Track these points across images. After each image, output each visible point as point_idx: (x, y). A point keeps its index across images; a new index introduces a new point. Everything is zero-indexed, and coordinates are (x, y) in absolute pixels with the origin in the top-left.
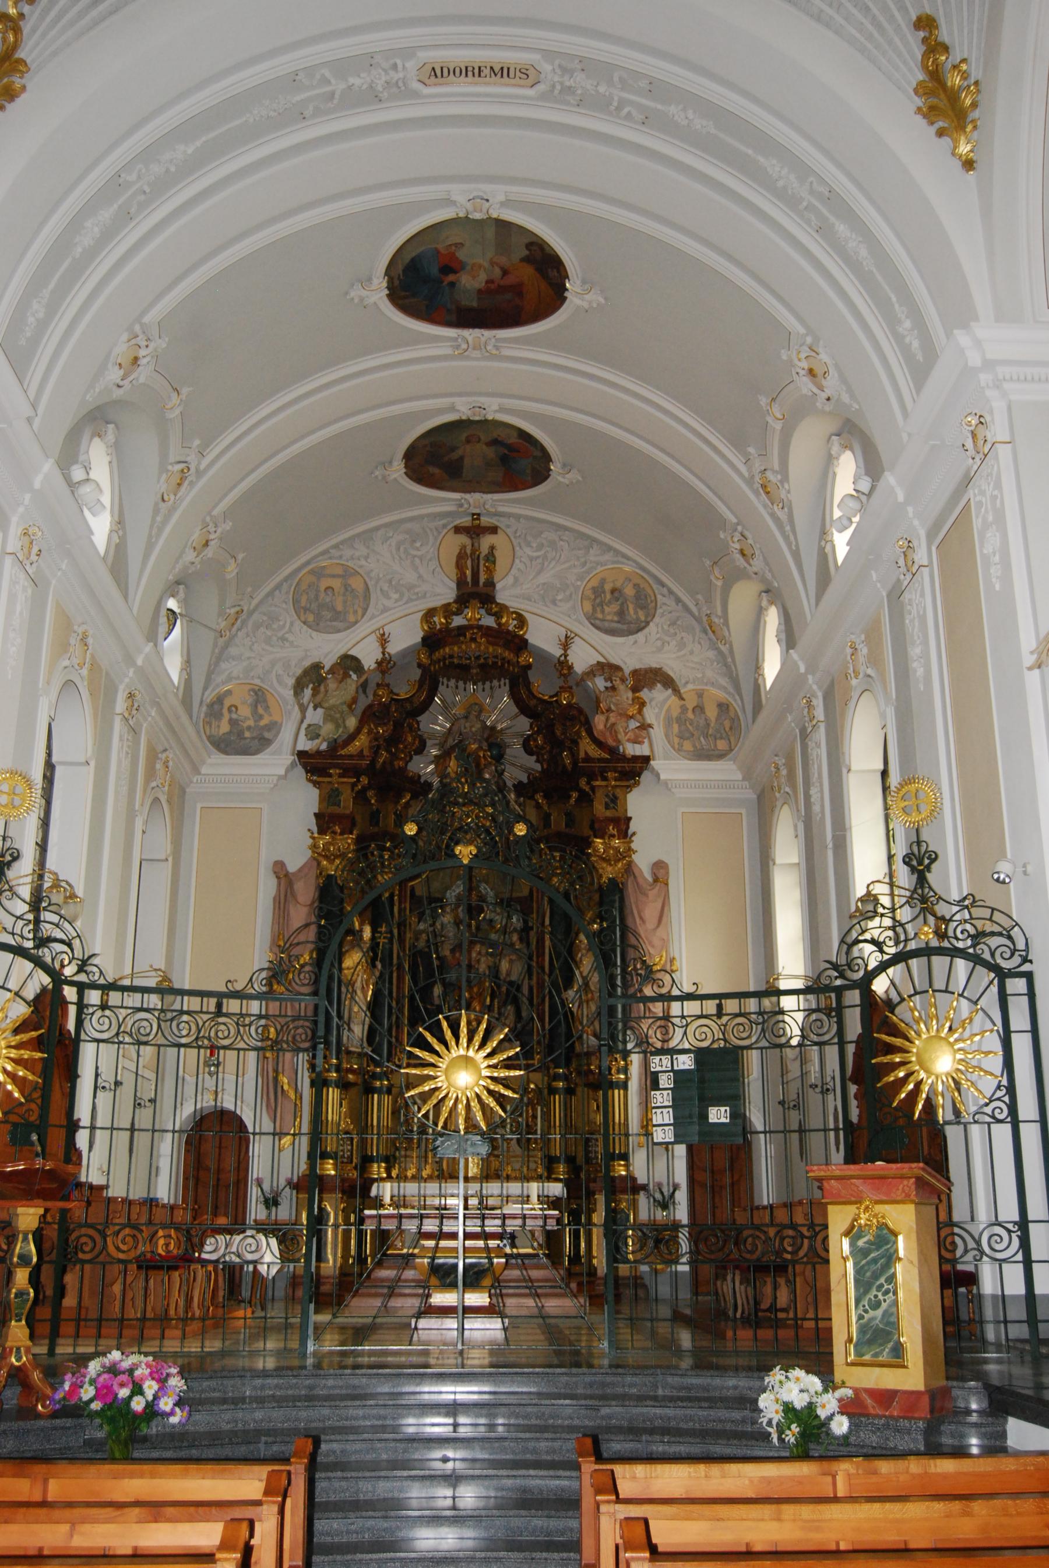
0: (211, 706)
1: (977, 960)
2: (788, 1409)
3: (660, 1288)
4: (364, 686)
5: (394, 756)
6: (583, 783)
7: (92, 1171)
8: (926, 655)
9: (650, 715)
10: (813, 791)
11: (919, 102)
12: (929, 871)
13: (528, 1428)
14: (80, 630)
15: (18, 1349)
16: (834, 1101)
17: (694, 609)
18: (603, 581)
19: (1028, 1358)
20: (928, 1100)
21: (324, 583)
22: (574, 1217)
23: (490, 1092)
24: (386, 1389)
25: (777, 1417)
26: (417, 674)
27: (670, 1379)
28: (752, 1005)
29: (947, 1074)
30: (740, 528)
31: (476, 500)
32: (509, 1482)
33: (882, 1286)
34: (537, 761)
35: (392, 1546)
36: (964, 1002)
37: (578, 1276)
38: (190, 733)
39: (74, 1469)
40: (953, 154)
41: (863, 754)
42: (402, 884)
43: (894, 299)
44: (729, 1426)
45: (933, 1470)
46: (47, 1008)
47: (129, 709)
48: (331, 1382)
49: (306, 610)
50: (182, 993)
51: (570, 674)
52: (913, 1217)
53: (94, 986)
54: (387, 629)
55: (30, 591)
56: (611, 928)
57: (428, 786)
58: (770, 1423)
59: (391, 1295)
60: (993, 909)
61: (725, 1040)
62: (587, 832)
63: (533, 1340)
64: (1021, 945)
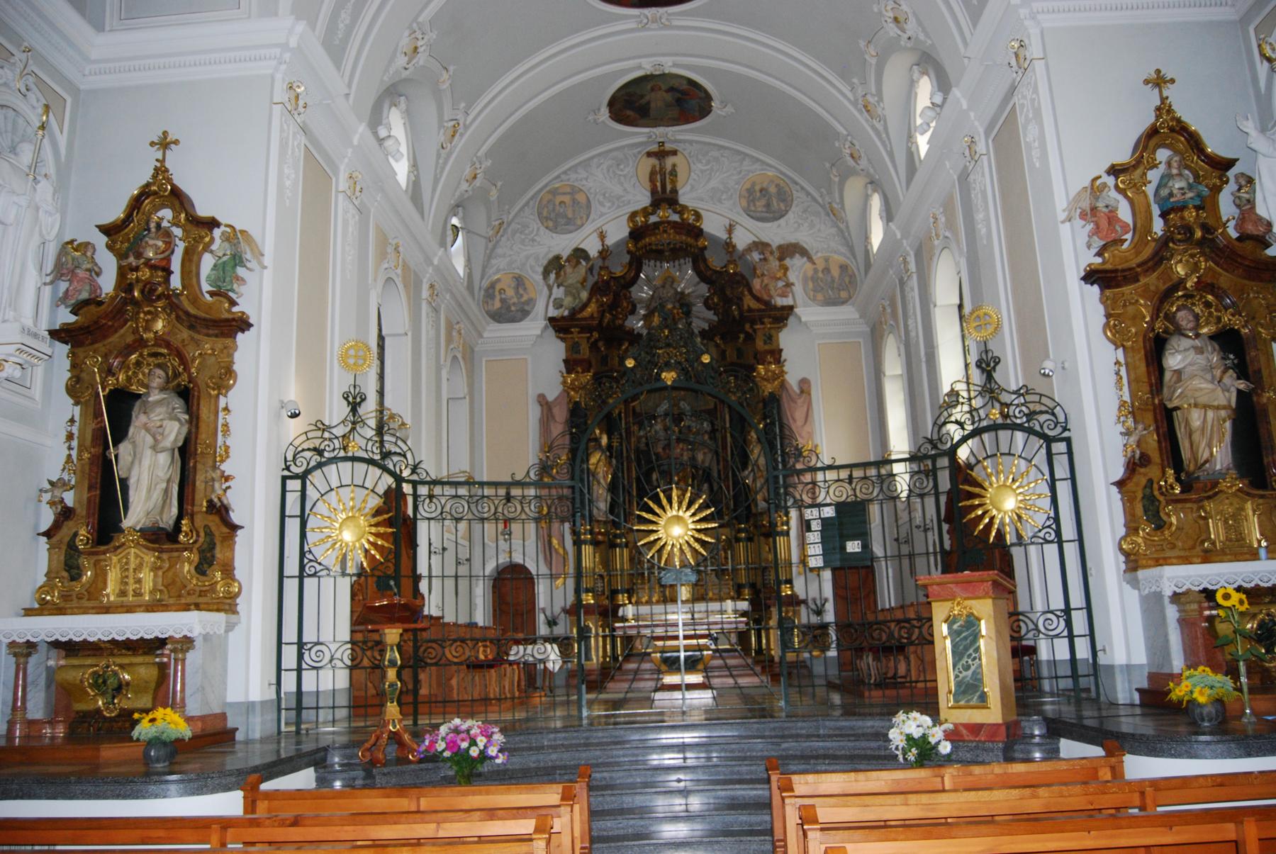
0: (487, 290)
1: (1030, 431)
2: (909, 738)
4: (591, 270)
5: (615, 317)
6: (747, 326)
7: (432, 608)
8: (987, 219)
9: (792, 276)
10: (910, 322)
13: (733, 759)
14: (394, 242)
16: (933, 537)
17: (820, 200)
18: (753, 184)
19: (1072, 700)
20: (998, 530)
21: (559, 199)
22: (757, 622)
23: (697, 540)
24: (636, 737)
25: (902, 744)
26: (627, 258)
27: (827, 723)
28: (872, 472)
31: (660, 132)
32: (723, 793)
35: (646, 836)
36: (1023, 462)
37: (763, 662)
38: (475, 310)
39: (435, 791)
41: (945, 292)
42: (626, 402)
44: (869, 752)
46: (393, 498)
47: (431, 295)
48: (600, 734)
49: (547, 219)
50: (482, 484)
53: (423, 483)
54: (604, 228)
56: (773, 423)
57: (640, 335)
58: (897, 748)
59: (633, 680)
62: (752, 361)
63: (735, 703)
64: (1062, 419)
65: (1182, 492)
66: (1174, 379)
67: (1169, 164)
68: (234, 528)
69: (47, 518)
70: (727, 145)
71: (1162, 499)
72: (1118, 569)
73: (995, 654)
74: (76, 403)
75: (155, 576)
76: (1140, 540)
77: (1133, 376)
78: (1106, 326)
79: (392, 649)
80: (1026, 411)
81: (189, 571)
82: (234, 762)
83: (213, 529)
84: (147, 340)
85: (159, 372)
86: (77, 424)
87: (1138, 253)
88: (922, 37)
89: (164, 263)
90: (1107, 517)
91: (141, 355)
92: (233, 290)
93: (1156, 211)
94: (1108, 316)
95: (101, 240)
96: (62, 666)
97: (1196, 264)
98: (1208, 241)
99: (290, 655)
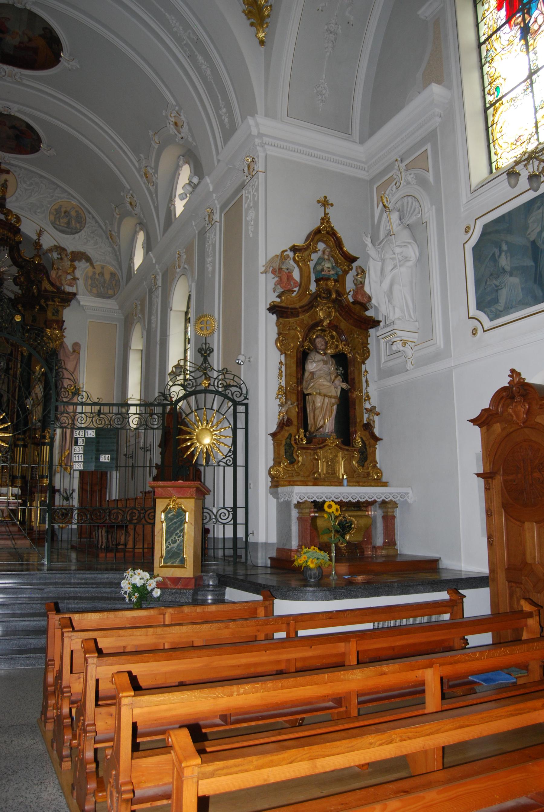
1: (226, 397)
2: (134, 586)
3: (63, 535)
6: (42, 301)
8: (214, 262)
9: (78, 273)
10: (153, 317)
11: (245, 7)
12: (209, 356)
17: (104, 227)
18: (61, 207)
27: (77, 575)
28: (115, 409)
29: (209, 445)
30: (131, 192)
33: (178, 533)
34: (20, 289)
40: (256, 36)
43: (220, 97)
44: (104, 595)
45: (206, 610)
51: (40, 248)
52: (194, 505)
60: (234, 375)
61: (111, 425)
64: (244, 392)
65: (306, 443)
66: (310, 377)
67: (324, 252)
70: (45, 175)
71: (295, 446)
72: (267, 485)
73: (193, 534)
76: (281, 469)
77: (288, 372)
78: (277, 340)
80: (225, 384)
87: (300, 300)
88: (190, 139)
90: (264, 454)
93: (313, 278)
94: (279, 334)
97: (330, 312)
98: (339, 303)
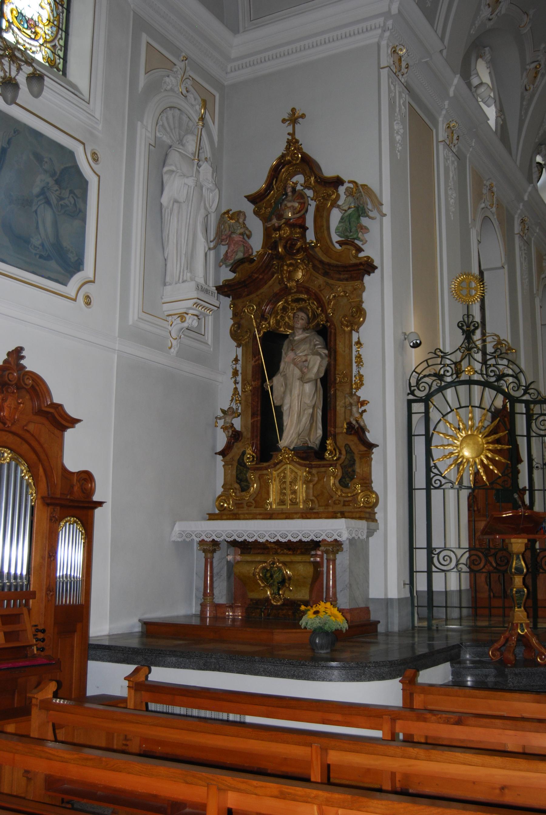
14: (488, 183)
15: (521, 624)
55: (456, 163)
68: (371, 446)
69: (222, 441)
74: (238, 346)
75: (307, 488)
79: (518, 558)
81: (334, 484)
82: (376, 652)
83: (353, 447)
84: (291, 289)
85: (302, 315)
86: (240, 362)
89: (300, 222)
91: (286, 302)
92: (358, 239)
95: (249, 208)
96: (238, 562)
99: (421, 558)
